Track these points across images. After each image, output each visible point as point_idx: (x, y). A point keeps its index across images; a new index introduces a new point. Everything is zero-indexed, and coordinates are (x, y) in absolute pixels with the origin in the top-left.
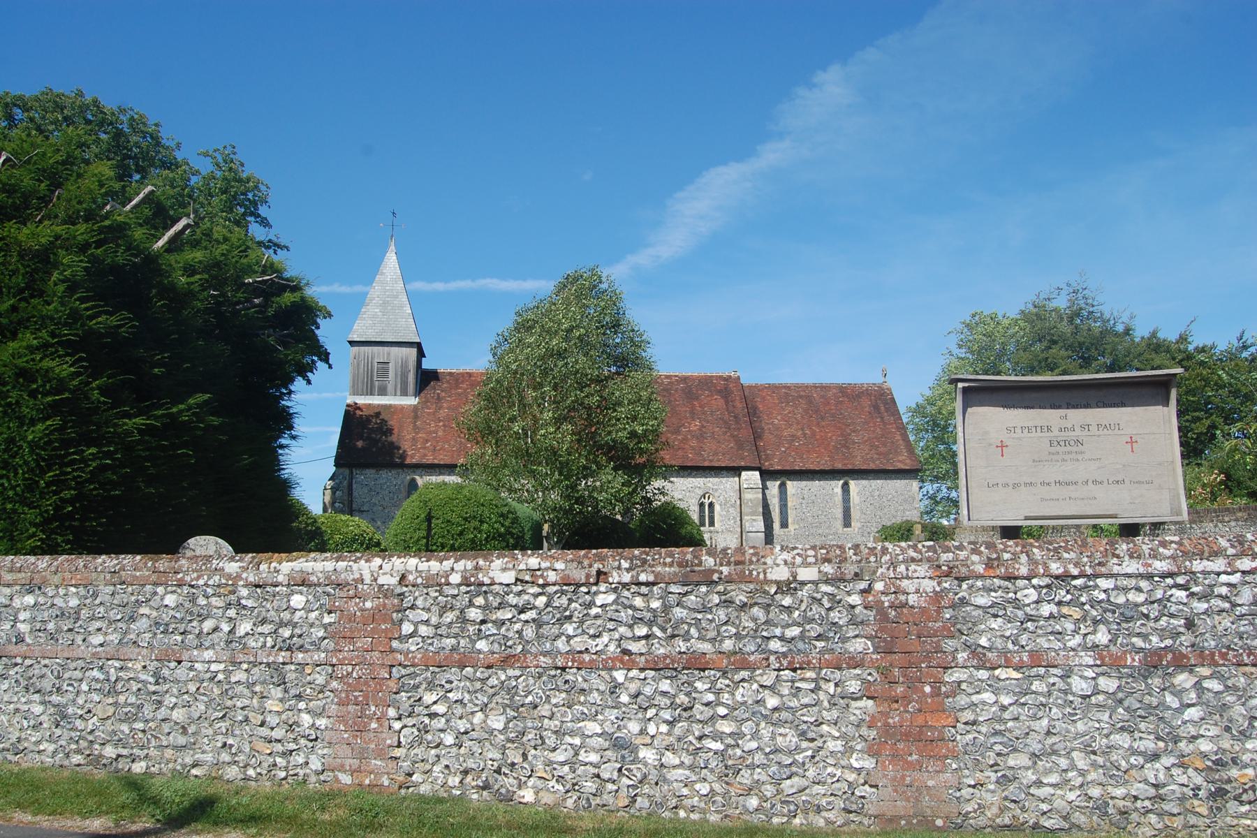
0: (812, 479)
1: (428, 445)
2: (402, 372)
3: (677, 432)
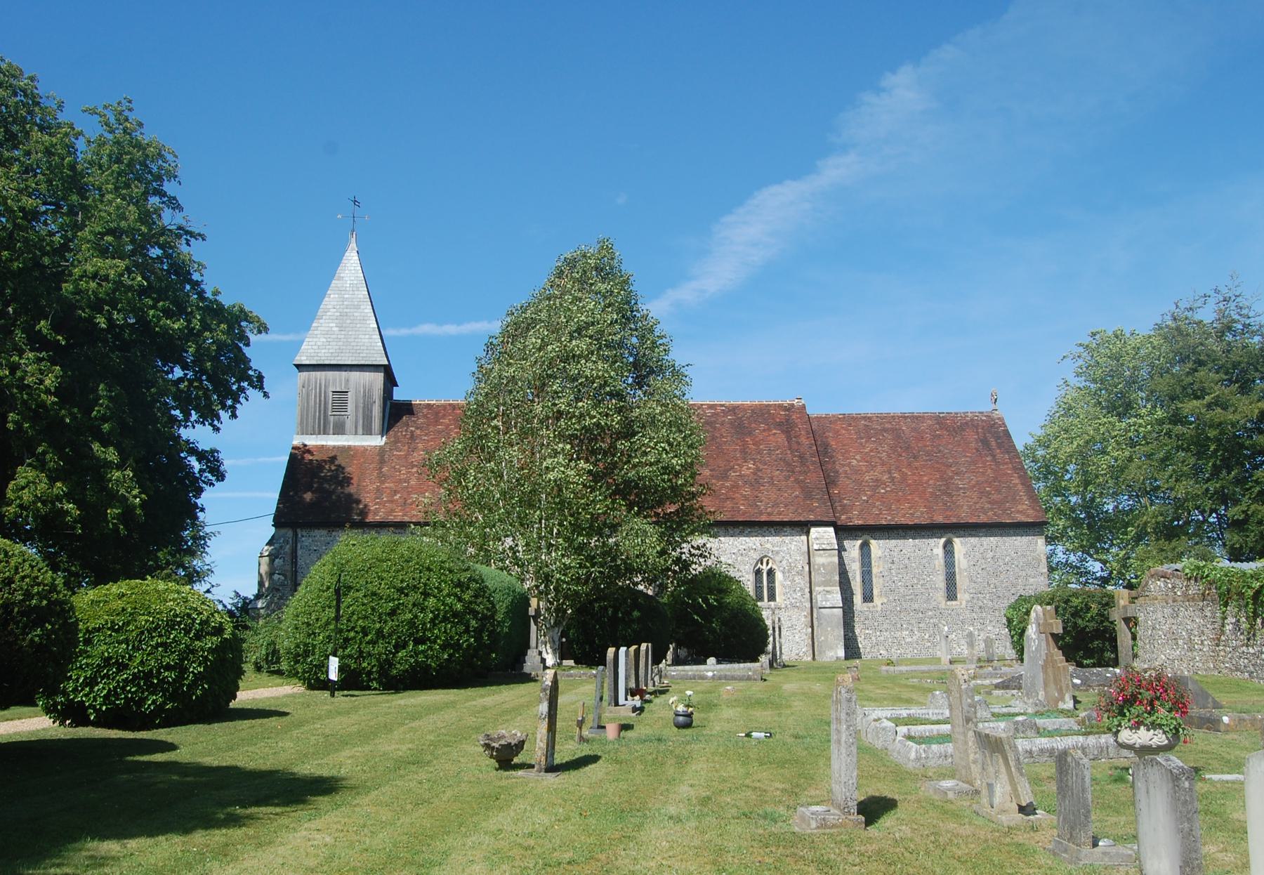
0: (904, 538)
1: (397, 497)
2: (364, 403)
3: (724, 476)
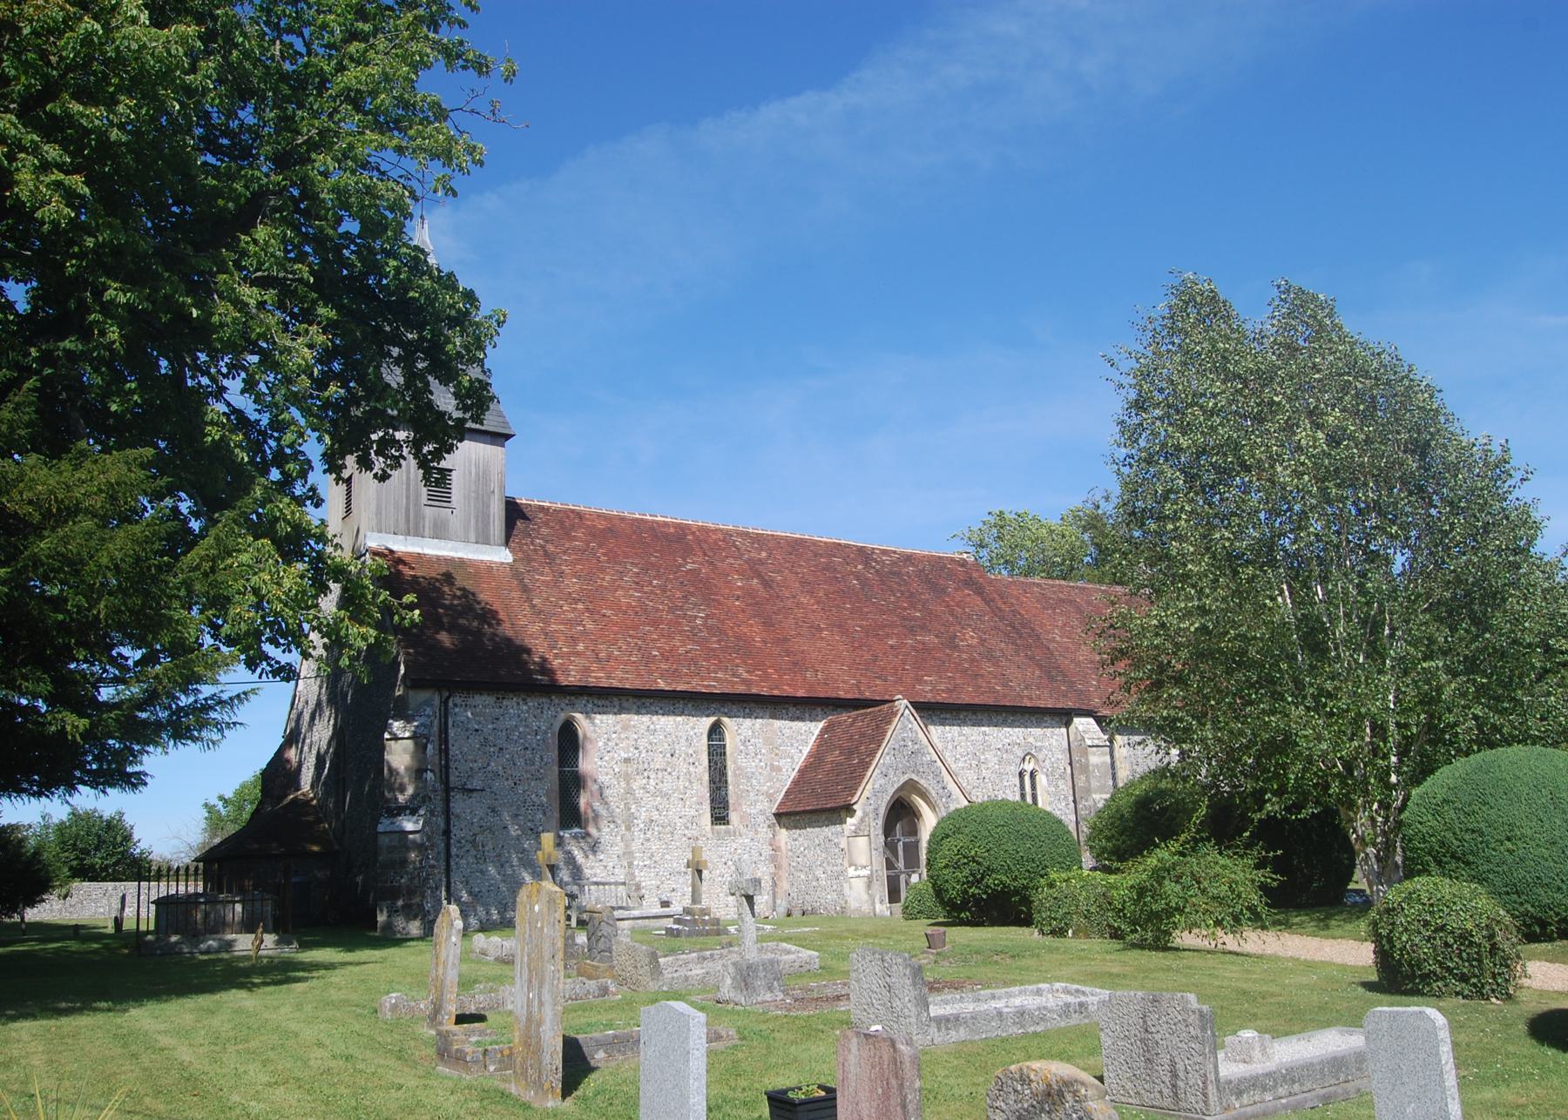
1: (581, 647)
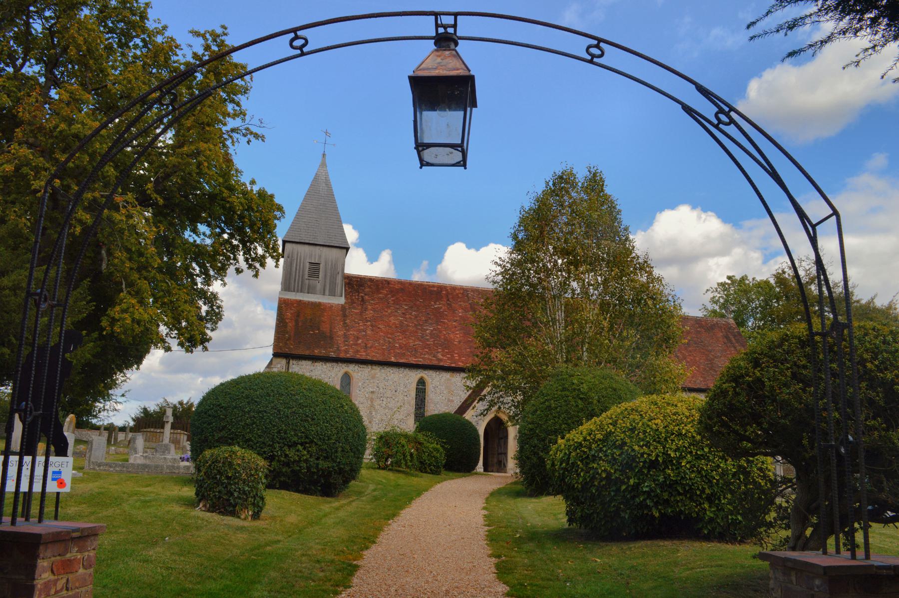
1: (360, 341)
